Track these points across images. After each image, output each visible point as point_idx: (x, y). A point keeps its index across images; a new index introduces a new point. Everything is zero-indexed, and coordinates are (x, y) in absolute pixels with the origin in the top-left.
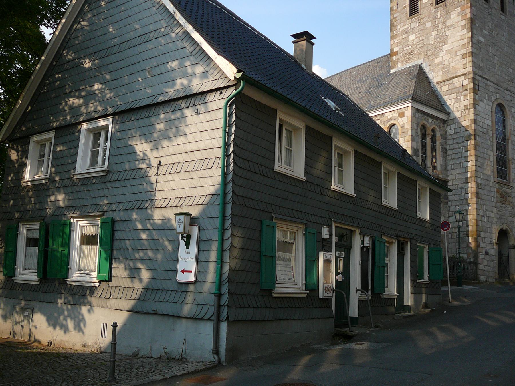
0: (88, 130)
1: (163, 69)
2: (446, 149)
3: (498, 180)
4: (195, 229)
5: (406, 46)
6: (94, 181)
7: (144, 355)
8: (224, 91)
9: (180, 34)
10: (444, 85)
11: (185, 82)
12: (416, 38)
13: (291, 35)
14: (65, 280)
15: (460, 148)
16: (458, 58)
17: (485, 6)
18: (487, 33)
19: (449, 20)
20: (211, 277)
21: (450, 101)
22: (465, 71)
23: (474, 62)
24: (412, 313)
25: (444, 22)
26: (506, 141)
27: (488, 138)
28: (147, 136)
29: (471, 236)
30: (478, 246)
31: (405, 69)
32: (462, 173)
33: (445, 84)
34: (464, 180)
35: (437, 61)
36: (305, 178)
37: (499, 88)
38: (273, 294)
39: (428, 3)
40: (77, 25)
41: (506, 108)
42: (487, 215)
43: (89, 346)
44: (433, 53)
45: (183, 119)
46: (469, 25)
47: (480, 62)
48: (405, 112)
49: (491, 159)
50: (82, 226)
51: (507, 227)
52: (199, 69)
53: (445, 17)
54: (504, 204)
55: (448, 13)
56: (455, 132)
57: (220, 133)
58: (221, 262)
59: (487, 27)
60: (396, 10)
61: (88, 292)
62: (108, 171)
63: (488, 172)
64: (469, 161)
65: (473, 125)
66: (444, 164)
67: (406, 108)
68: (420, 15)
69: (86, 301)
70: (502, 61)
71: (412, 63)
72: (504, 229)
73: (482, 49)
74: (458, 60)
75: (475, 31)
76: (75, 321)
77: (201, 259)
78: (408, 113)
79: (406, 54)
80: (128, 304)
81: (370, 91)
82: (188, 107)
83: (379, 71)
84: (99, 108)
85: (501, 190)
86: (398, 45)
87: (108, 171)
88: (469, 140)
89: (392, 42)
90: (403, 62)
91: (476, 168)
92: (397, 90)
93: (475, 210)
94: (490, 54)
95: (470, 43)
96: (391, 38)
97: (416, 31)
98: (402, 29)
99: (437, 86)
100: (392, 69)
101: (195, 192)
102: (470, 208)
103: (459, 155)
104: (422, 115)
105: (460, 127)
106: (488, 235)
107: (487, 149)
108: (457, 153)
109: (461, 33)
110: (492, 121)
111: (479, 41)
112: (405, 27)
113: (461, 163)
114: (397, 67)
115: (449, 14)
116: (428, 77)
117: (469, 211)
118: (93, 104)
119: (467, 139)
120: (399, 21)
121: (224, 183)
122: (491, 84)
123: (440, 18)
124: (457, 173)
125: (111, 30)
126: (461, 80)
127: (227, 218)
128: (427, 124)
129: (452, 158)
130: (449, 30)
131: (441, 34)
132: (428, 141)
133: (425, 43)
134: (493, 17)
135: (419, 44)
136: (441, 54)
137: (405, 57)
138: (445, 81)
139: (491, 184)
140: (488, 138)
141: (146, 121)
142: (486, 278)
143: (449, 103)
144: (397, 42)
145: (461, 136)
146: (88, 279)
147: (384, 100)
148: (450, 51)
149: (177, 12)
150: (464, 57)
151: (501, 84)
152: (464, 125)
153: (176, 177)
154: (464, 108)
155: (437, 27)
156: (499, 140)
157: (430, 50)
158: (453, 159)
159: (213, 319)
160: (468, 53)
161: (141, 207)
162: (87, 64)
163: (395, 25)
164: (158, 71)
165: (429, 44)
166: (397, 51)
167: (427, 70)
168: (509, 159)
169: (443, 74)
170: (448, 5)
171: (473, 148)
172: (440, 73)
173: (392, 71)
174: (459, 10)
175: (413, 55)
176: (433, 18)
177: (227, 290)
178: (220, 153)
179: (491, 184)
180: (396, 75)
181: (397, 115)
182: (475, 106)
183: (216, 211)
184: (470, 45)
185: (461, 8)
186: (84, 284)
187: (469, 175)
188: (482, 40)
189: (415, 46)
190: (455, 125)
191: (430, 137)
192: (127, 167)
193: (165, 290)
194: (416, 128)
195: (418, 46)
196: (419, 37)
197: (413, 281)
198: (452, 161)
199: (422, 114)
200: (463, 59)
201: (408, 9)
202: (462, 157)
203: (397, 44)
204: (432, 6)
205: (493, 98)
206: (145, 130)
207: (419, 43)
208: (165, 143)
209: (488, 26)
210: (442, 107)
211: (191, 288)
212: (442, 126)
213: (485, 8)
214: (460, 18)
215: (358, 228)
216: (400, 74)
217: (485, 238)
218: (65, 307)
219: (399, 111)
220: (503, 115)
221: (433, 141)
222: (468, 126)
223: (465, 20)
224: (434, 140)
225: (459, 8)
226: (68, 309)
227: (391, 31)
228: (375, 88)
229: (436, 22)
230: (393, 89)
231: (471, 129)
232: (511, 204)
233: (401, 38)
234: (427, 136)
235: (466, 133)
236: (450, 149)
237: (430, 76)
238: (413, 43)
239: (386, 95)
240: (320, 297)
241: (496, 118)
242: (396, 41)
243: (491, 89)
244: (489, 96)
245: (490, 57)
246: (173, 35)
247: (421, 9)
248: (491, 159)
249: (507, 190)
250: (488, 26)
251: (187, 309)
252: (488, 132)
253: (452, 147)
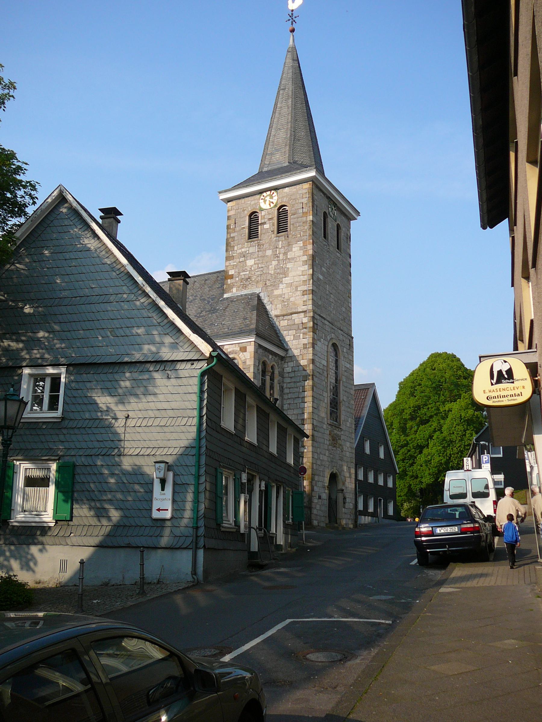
0: (30, 375)
1: (127, 331)
2: (282, 387)
3: (331, 422)
4: (171, 475)
5: (244, 271)
6: (44, 427)
7: (116, 583)
8: (195, 363)
9: (146, 304)
10: (283, 320)
11: (154, 349)
12: (255, 264)
13: (167, 273)
14: (8, 521)
15: (297, 388)
16: (299, 293)
17: (324, 243)
18: (325, 270)
19: (290, 253)
20: (188, 514)
21: (289, 337)
22: (305, 308)
23: (314, 300)
24: (283, 552)
25: (285, 254)
26: (338, 382)
28: (110, 391)
29: (306, 480)
30: (312, 490)
31: (242, 296)
33: (284, 319)
34: (300, 421)
35: (276, 292)
36: (234, 432)
38: (221, 528)
39: (269, 229)
40: (11, 266)
41: (339, 348)
42: (321, 459)
43: (43, 583)
44: (273, 284)
45: (151, 381)
46: (311, 262)
49: (326, 401)
50: (26, 469)
51: (337, 471)
52: (168, 340)
53: (286, 248)
54: (334, 447)
55: (289, 245)
57: (195, 398)
58: (196, 501)
59: (326, 265)
60: (234, 229)
61: (38, 533)
62: (62, 417)
63: (323, 415)
64: (306, 402)
65: (311, 365)
66: (281, 404)
67: (249, 343)
68: (260, 240)
69: (36, 541)
72: (334, 472)
73: (321, 287)
74: (299, 296)
75: (315, 269)
76: (21, 560)
77: (177, 499)
78: (251, 349)
79: (242, 279)
80: (96, 541)
81: (201, 315)
82: (158, 371)
83: (209, 291)
84: (47, 356)
88: (307, 380)
89: (228, 264)
90: (239, 287)
91: (313, 409)
92: (237, 321)
93: (311, 453)
94: (327, 292)
95: (311, 280)
96: (226, 259)
97: (254, 257)
99: (275, 319)
100: (226, 293)
101: (169, 444)
102: (305, 450)
103: (296, 395)
104: (263, 351)
105: (298, 366)
106: (321, 479)
107: (323, 391)
109: (302, 268)
111: (318, 278)
112: (243, 250)
115: (291, 246)
116: (266, 309)
117: (304, 453)
118: (39, 352)
119: (305, 378)
120: (237, 242)
121: (199, 438)
123: (281, 248)
124: (293, 414)
125: (58, 281)
126: (301, 317)
127: (201, 467)
128: (267, 360)
130: (290, 262)
131: (281, 265)
132: (268, 378)
133: (264, 272)
134: (330, 255)
135: (257, 272)
136: (281, 286)
137: (242, 282)
138: (284, 316)
139: (325, 427)
140: (323, 378)
141: (110, 376)
142: (318, 523)
143: (287, 339)
145: (299, 375)
146: (37, 520)
148: (290, 285)
149: (146, 285)
150: (304, 293)
151: (336, 323)
152: (302, 364)
154: (302, 347)
155: (278, 257)
157: (269, 280)
158: (289, 399)
159: (191, 547)
160: (309, 290)
161: (108, 454)
162: (28, 310)
163: (232, 245)
164: (121, 332)
166: (233, 275)
167: (265, 301)
169: (282, 307)
170: (290, 236)
171: (311, 389)
172: (279, 306)
173: (226, 296)
174: (301, 244)
175: (251, 282)
176: (274, 246)
177: (203, 524)
178: (196, 413)
179: (325, 427)
180: (232, 301)
181: (239, 349)
182: (313, 345)
183: (192, 461)
184: (311, 283)
185: (303, 243)
186: (34, 524)
187: (306, 416)
188: (321, 277)
189: (253, 273)
190: (292, 363)
191: (270, 374)
192: (87, 416)
193: (144, 526)
194: (258, 365)
195: (257, 273)
196: (258, 264)
197: (284, 522)
198: (288, 400)
199: (263, 350)
200: (303, 295)
202: (298, 397)
203: (234, 267)
204: (274, 233)
205: (329, 338)
206: (109, 385)
207: (258, 270)
208: (133, 400)
209: (326, 264)
210: (280, 343)
211: (168, 524)
212: (280, 363)
213: (325, 245)
214: (301, 253)
215: (258, 473)
216: (236, 301)
218: (6, 548)
219: (241, 345)
221: (272, 379)
222: (306, 365)
223: (307, 255)
224: (272, 377)
225: (302, 242)
226: (10, 550)
227: (227, 251)
228: (207, 313)
230: (231, 318)
231: (310, 369)
232: (340, 447)
233: (238, 260)
234: (266, 373)
235: (304, 373)
236: (287, 388)
237: (268, 307)
238: (251, 268)
239: (224, 324)
240: (241, 532)
242: (232, 263)
246: (138, 303)
247: (261, 234)
248: (326, 401)
249: (338, 432)
250: (326, 264)
251: (164, 541)
252: (323, 372)
253: (289, 386)
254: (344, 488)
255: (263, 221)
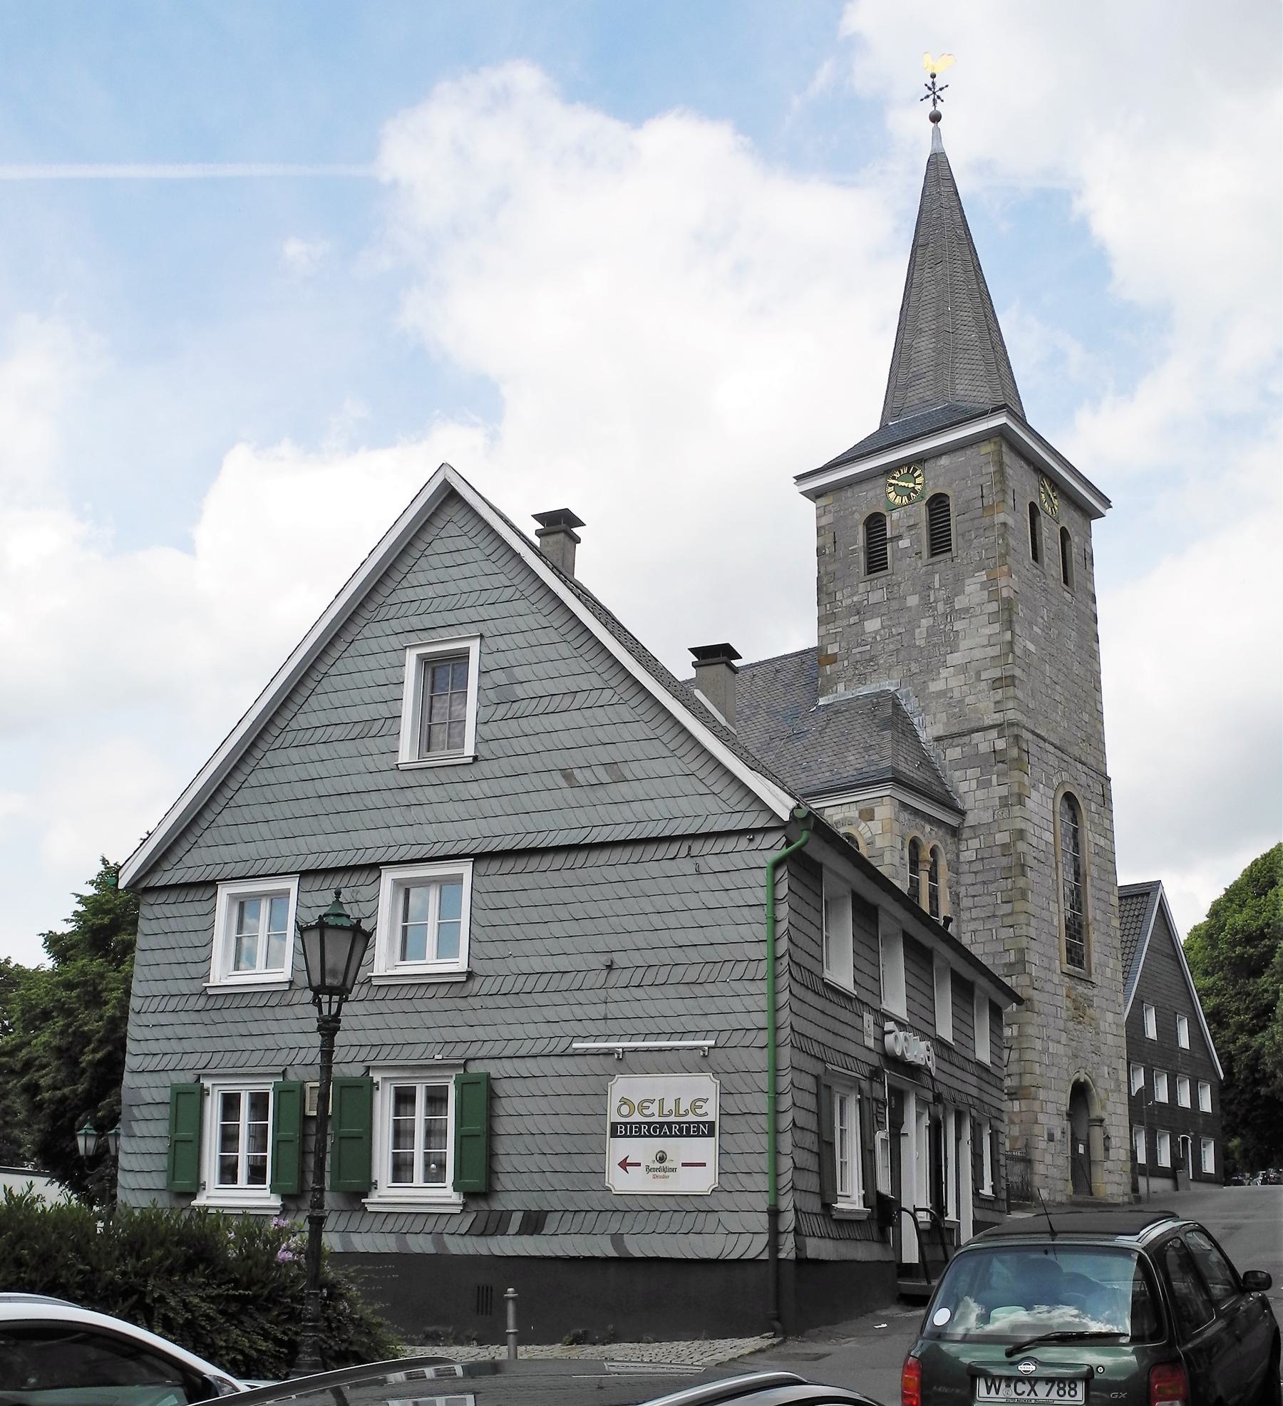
8: (758, 838)
10: (952, 746)
12: (883, 628)
16: (983, 685)
25: (949, 601)
27: (1047, 871)
32: (996, 952)
35: (934, 687)
37: (1066, 758)
47: (1030, 699)
48: (876, 809)
54: (1080, 1023)
56: (979, 857)
59: (1040, 620)
70: (1069, 697)
71: (874, 685)
72: (1082, 1080)
79: (857, 662)
85: (1074, 993)
86: (838, 639)
87: (470, 975)
94: (1048, 681)
98: (847, 602)
104: (911, 817)
108: (984, 907)
109: (988, 631)
110: (1054, 834)
112: (855, 599)
113: (994, 930)
114: (836, 692)
122: (1051, 749)
123: (938, 589)
128: (921, 837)
129: (973, 917)
139: (1056, 979)
144: (835, 631)
147: (819, 776)
148: (963, 669)
150: (997, 685)
153: (654, 992)
156: (1068, 877)
158: (974, 919)
165: (915, 646)
167: (909, 706)
168: (1088, 921)
172: (943, 717)
175: (876, 667)
181: (856, 814)
188: (1032, 647)
196: (890, 627)
198: (972, 923)
201: (862, 557)
202: (994, 916)
205: (1055, 782)
209: (1042, 618)
217: (1046, 1102)
219: (862, 806)
220: (1075, 819)
229: (929, 596)
238: (875, 638)
241: (1062, 826)
243: (1052, 760)
244: (1048, 778)
245: (1047, 685)
249: (1086, 991)
250: (1042, 618)
253: (971, 891)
254: (1104, 1115)
255: (895, 534)
